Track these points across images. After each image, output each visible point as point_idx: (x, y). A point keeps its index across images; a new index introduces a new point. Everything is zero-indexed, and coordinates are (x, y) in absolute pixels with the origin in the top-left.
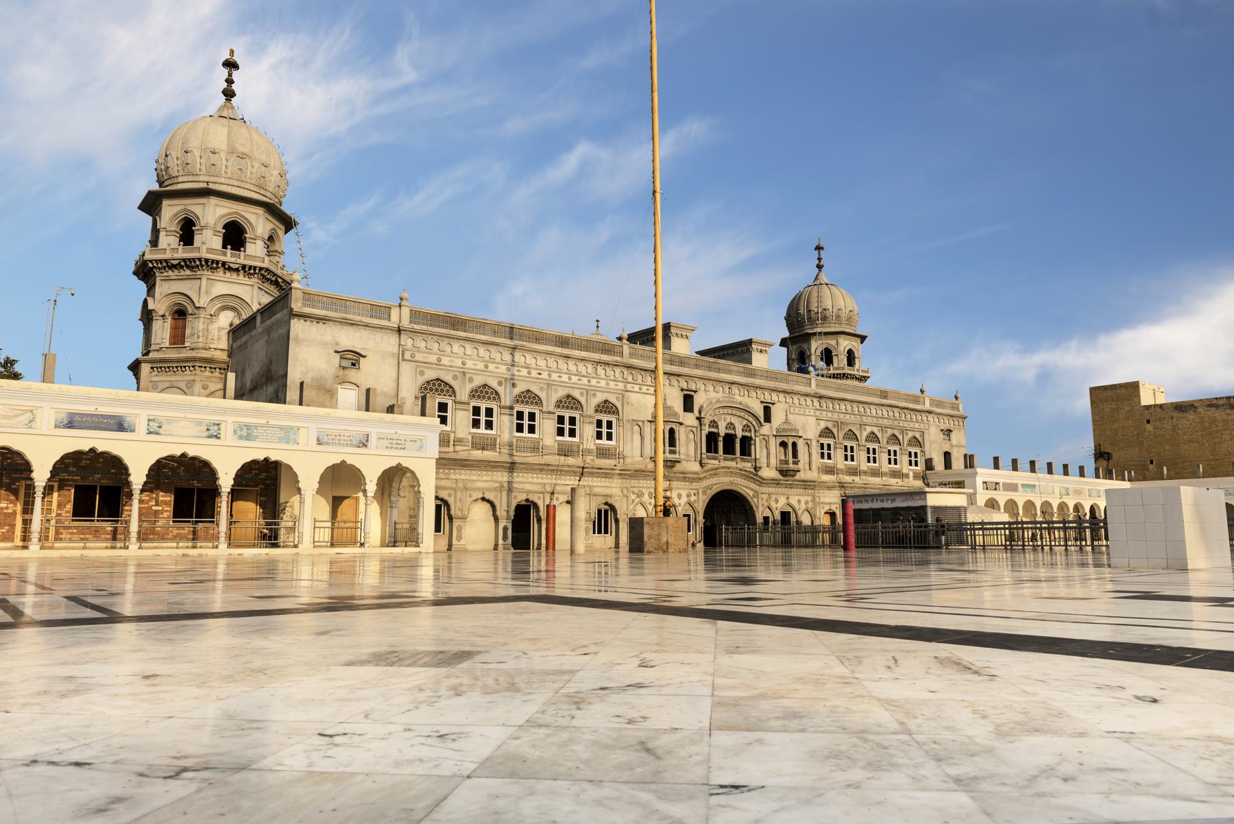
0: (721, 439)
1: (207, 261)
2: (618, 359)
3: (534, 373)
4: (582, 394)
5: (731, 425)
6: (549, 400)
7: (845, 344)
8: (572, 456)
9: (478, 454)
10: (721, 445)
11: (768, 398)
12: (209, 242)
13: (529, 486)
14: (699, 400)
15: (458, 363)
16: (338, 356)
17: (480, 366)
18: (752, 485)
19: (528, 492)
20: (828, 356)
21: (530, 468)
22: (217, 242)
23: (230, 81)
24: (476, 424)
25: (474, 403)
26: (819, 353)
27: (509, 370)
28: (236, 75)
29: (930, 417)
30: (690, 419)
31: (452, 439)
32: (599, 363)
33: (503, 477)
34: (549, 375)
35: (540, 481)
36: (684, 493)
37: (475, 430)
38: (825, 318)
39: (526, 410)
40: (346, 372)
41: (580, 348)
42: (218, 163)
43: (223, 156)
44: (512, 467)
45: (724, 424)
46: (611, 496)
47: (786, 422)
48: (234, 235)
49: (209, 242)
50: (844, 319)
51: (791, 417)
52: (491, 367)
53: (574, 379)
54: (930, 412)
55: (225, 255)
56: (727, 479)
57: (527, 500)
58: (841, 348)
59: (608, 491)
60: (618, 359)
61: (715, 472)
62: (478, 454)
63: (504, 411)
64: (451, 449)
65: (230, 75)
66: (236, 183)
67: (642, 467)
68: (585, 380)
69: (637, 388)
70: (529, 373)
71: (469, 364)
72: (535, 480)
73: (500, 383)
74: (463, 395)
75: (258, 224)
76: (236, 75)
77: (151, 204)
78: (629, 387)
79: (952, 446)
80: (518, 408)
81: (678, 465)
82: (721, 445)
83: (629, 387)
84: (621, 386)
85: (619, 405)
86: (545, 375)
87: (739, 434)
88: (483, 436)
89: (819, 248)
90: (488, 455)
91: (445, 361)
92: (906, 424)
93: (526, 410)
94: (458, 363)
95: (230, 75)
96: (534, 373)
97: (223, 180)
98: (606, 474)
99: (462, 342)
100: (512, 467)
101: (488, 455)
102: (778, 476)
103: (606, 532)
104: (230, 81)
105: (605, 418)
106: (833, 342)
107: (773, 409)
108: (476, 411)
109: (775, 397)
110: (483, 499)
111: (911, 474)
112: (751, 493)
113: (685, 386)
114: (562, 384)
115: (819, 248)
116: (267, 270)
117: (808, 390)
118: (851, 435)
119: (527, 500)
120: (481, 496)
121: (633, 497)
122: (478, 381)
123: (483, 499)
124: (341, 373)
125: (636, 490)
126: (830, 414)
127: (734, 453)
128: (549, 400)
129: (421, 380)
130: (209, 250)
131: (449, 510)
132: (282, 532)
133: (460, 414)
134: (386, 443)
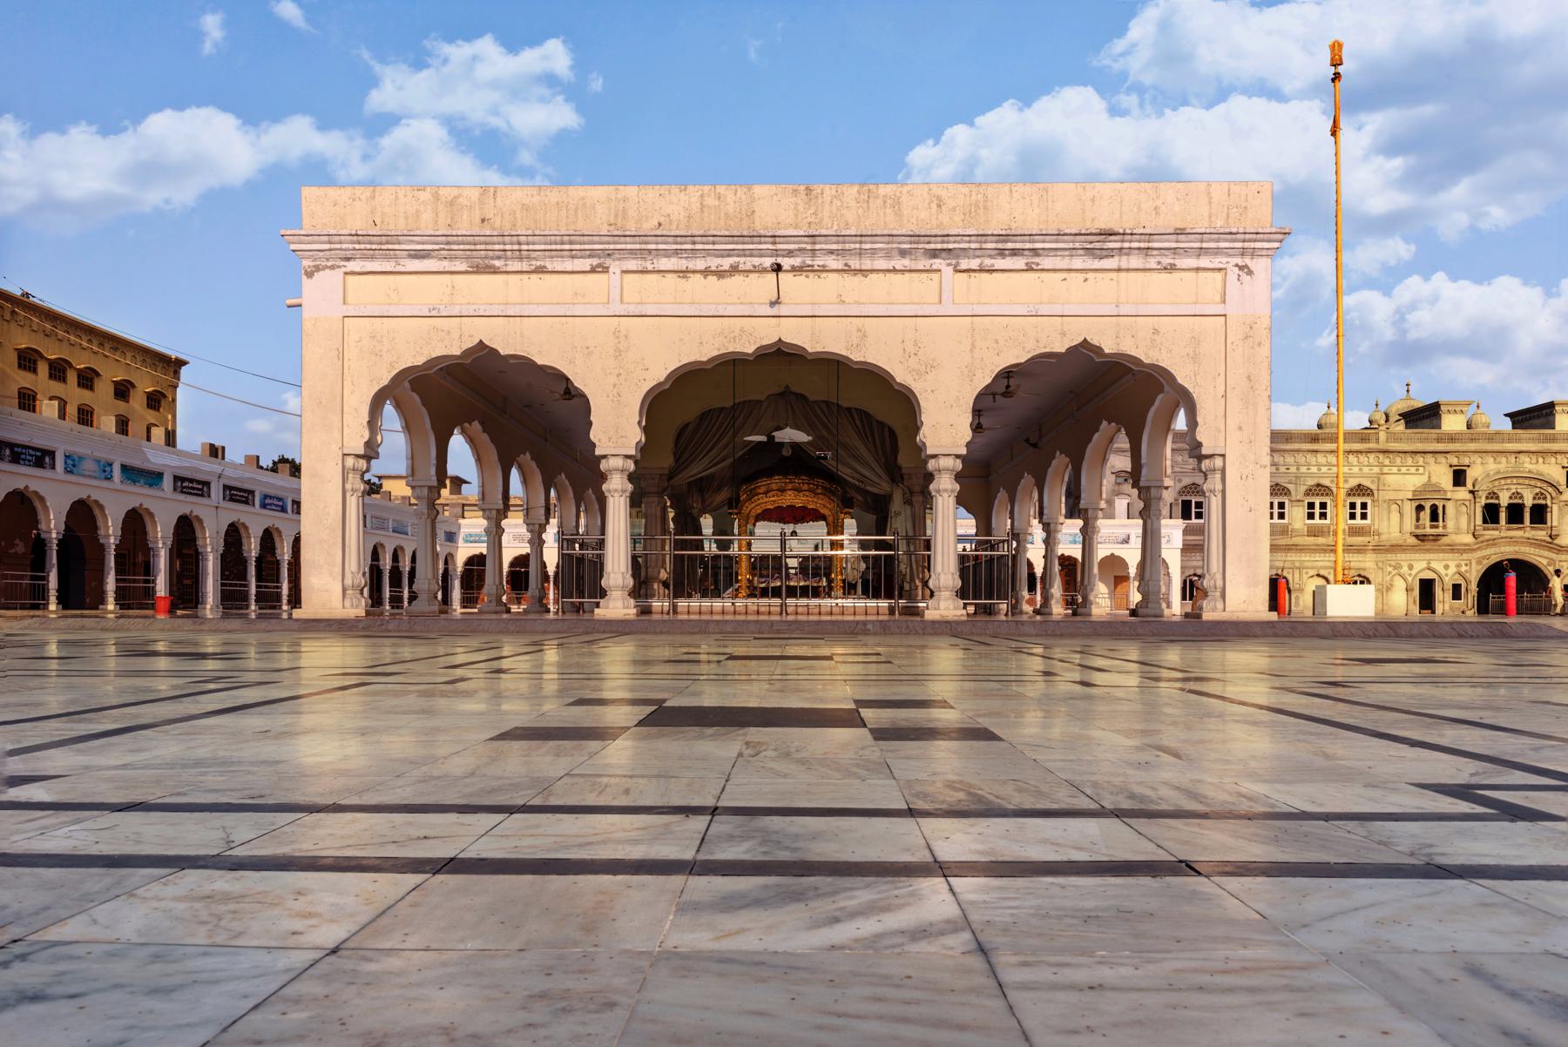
5: (1518, 495)
14: (1471, 475)
18: (1546, 553)
80: (1352, 499)
87: (1529, 501)
112: (1545, 562)
113: (1455, 461)
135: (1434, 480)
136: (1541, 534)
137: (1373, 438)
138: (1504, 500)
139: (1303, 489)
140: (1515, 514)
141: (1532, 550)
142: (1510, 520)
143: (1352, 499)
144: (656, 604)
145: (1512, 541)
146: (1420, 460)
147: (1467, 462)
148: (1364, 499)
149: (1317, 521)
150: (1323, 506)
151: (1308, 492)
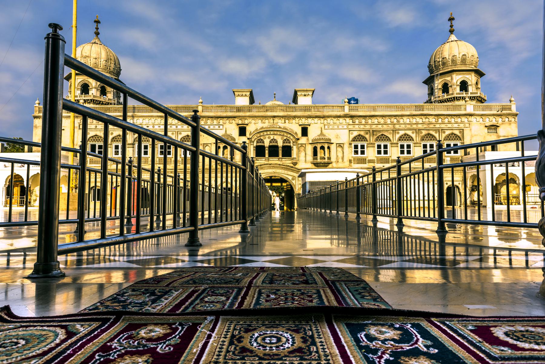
5: (274, 140)
7: (457, 79)
10: (267, 152)
11: (304, 121)
12: (456, 91)
14: (250, 129)
18: (290, 173)
20: (445, 88)
24: (379, 152)
25: (423, 143)
26: (440, 87)
28: (99, 26)
29: (472, 119)
37: (357, 156)
38: (444, 64)
39: (405, 144)
48: (464, 86)
49: (456, 91)
51: (324, 132)
54: (471, 115)
55: (463, 94)
65: (451, 23)
75: (471, 78)
80: (379, 143)
82: (267, 152)
87: (280, 144)
89: (97, 22)
93: (405, 144)
95: (451, 23)
99: (420, 117)
104: (451, 26)
105: (359, 144)
106: (449, 79)
108: (402, 146)
112: (290, 178)
113: (240, 122)
115: (451, 19)
116: (480, 97)
117: (342, 113)
118: (383, 137)
126: (362, 127)
127: (264, 156)
131: (459, 190)
132: (32, 201)
133: (371, 149)
135: (228, 133)
136: (287, 162)
137: (463, 108)
138: (267, 143)
139: (398, 136)
140: (274, 151)
141: (286, 172)
142: (271, 155)
143: (379, 143)
144: (225, 252)
145: (271, 166)
146: (221, 122)
147: (246, 122)
148: (385, 143)
149: (382, 155)
150: (363, 147)
151: (400, 139)
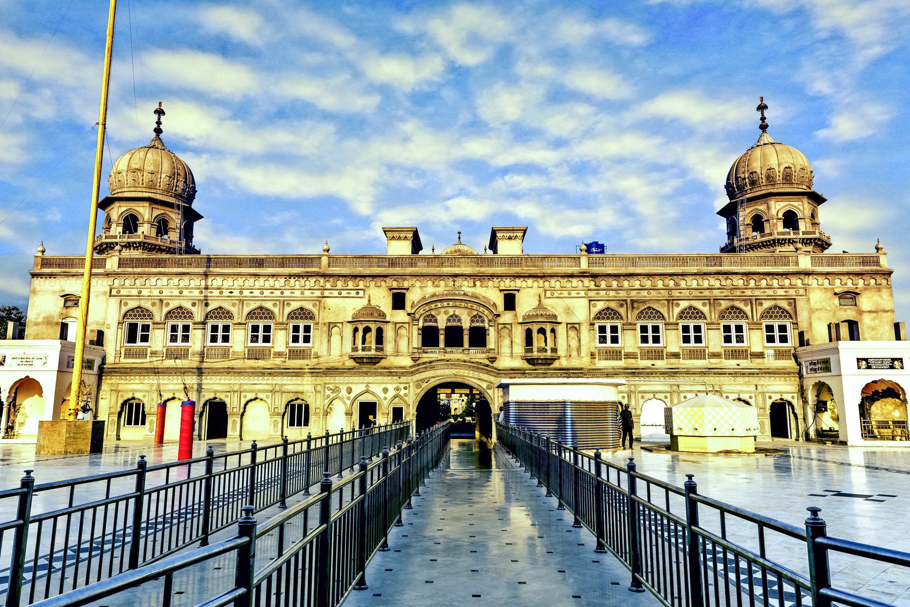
0: (442, 332)
1: (779, 240)
2: (875, 268)
3: (226, 293)
4: (275, 305)
6: (239, 313)
7: (777, 207)
8: (263, 359)
9: (170, 363)
10: (442, 338)
11: (507, 284)
12: (778, 229)
13: (215, 386)
14: (413, 297)
15: (156, 292)
16: (63, 299)
17: (176, 292)
19: (216, 392)
21: (216, 372)
22: (780, 227)
23: (159, 123)
25: (724, 323)
27: (201, 293)
28: (163, 118)
29: (812, 281)
30: (400, 316)
31: (149, 352)
32: (290, 276)
33: (192, 380)
34: (241, 293)
35: (227, 382)
36: (391, 388)
38: (753, 183)
39: (691, 324)
40: (69, 310)
41: (59, 266)
42: (122, 179)
43: (124, 174)
44: (200, 372)
45: (445, 317)
46: (302, 393)
47: (540, 306)
48: (790, 219)
50: (779, 178)
52: (186, 292)
53: (267, 293)
56: (448, 372)
57: (781, 399)
58: (774, 212)
59: (300, 388)
60: (875, 268)
61: (430, 365)
62: (170, 363)
63: (197, 326)
64: (148, 359)
65: (159, 119)
66: (133, 189)
67: (339, 365)
68: (278, 293)
69: (336, 293)
70: (221, 293)
71: (166, 292)
72: (222, 382)
73: (194, 305)
74: (158, 316)
75: (802, 207)
76: (163, 118)
77: (729, 212)
78: (326, 293)
79: (861, 312)
81: (383, 361)
82: (442, 338)
83: (326, 293)
84: (318, 293)
85: (315, 310)
86: (236, 293)
87: (466, 324)
88: (178, 349)
90: (179, 363)
91: (145, 292)
92: (757, 293)
93: (691, 324)
94: (156, 292)
95: (159, 119)
96: (226, 293)
97: (126, 189)
98: (298, 373)
100: (200, 372)
101: (179, 363)
102: (526, 365)
103: (143, 423)
104: (159, 123)
105: (180, 324)
106: (763, 207)
107: (518, 296)
109: (519, 283)
110: (739, 399)
111: (772, 352)
113: (395, 285)
114: (254, 298)
117: (575, 270)
119: (781, 399)
120: (736, 396)
121: (328, 392)
122: (173, 304)
123: (739, 399)
124: (65, 311)
125: (331, 386)
126: (612, 293)
128: (239, 313)
129: (124, 309)
130: (778, 234)
134: (18, 361)
